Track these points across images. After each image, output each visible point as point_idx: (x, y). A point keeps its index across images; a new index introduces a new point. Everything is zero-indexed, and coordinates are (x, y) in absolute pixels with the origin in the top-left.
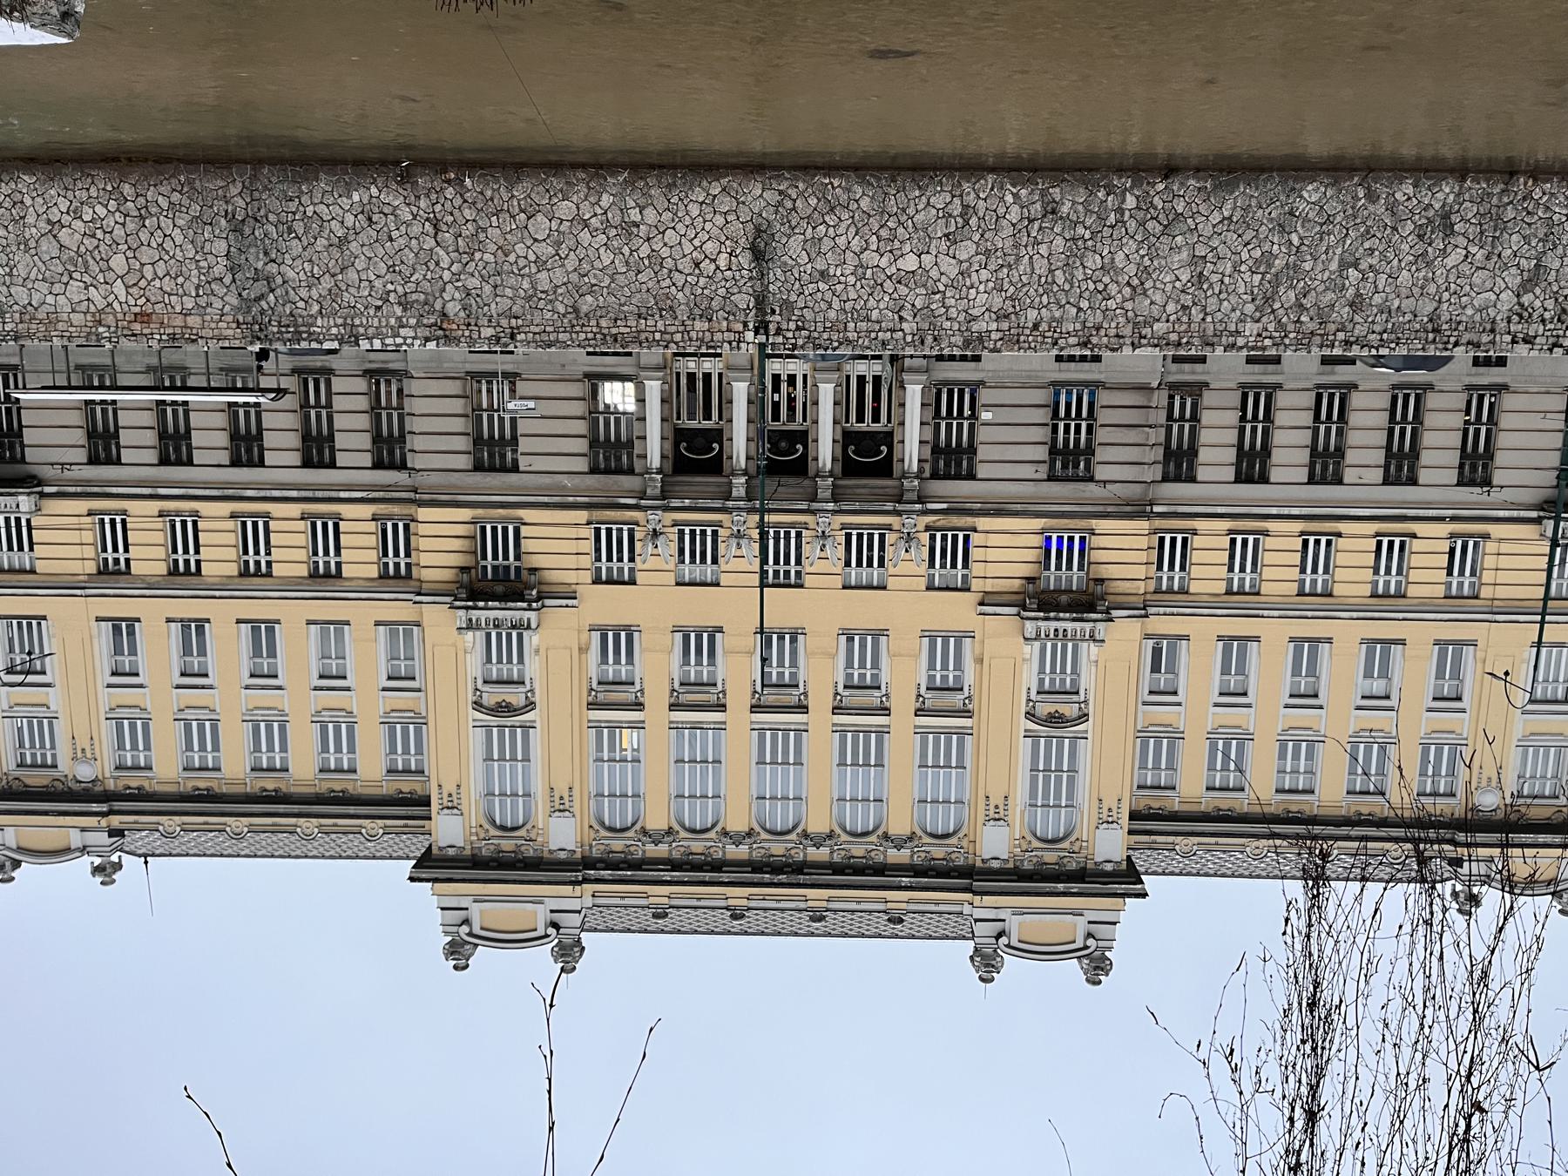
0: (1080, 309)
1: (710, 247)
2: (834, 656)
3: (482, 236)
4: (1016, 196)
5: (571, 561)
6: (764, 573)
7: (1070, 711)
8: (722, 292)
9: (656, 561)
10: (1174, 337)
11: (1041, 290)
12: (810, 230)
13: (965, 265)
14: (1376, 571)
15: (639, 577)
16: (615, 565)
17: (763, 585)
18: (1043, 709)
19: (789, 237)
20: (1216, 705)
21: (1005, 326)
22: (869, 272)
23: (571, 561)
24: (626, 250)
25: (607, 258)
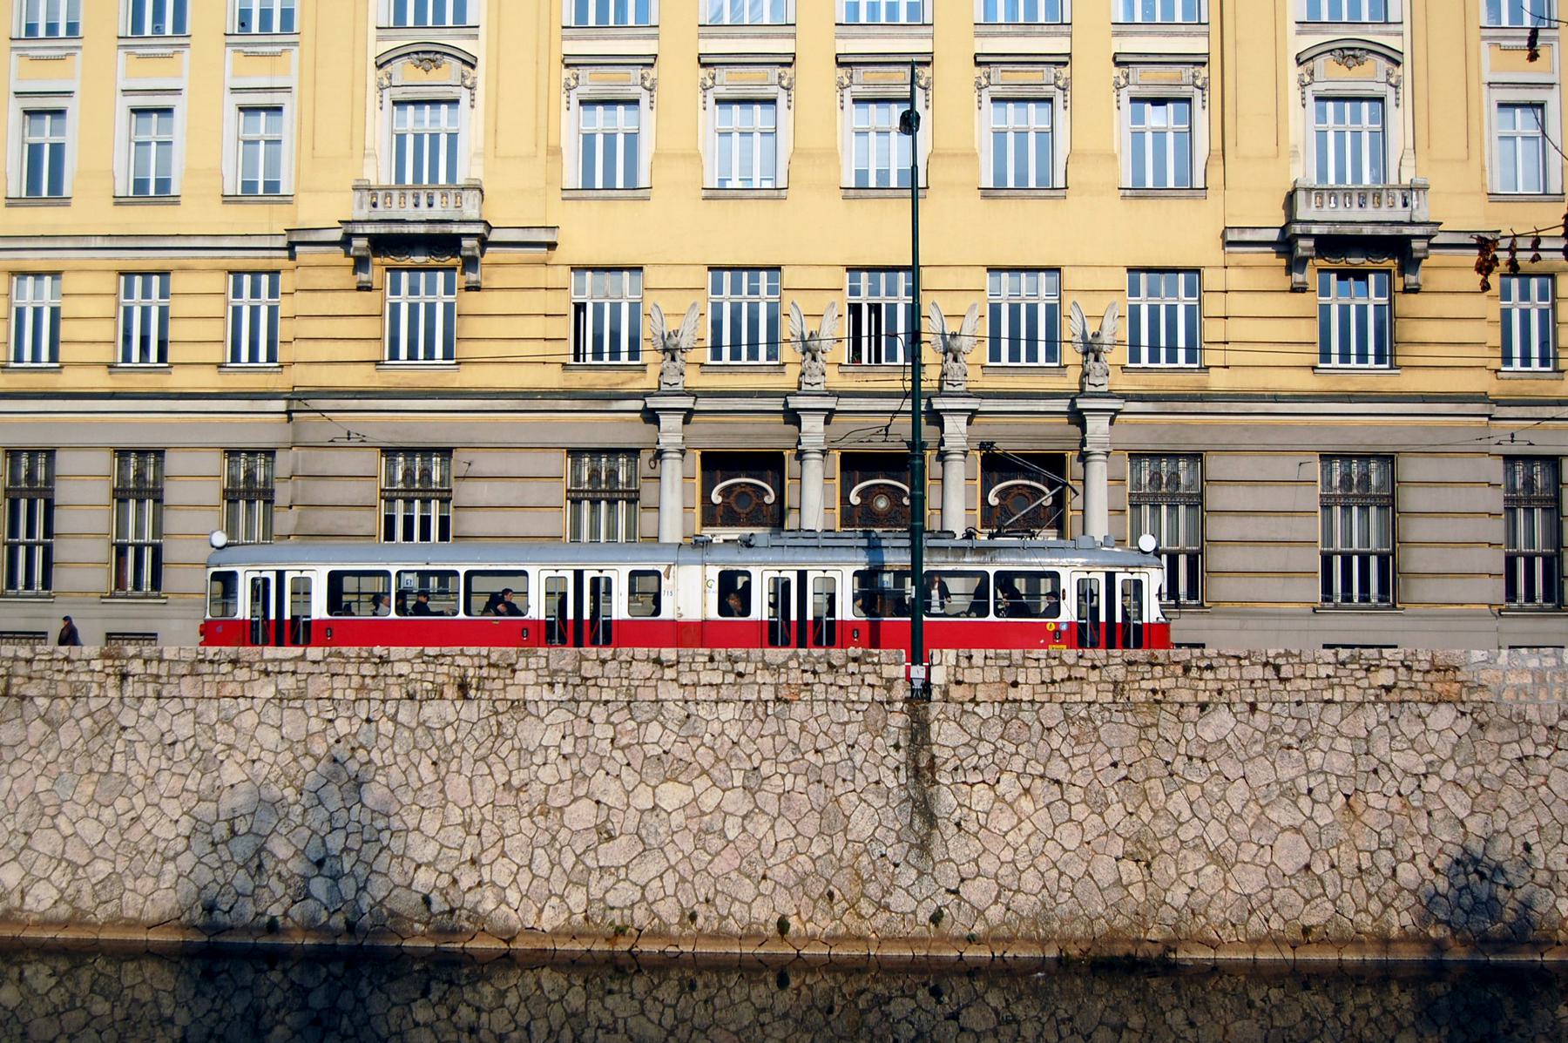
0: (393, 719)
1: (1004, 821)
2: (797, 152)
3: (1388, 836)
4: (503, 901)
5: (1237, 304)
6: (915, 290)
7: (404, 72)
8: (984, 749)
9: (1099, 306)
10: (243, 674)
11: (457, 749)
12: (838, 847)
13: (581, 791)
14: (164, 313)
15: (1124, 279)
16: (422, 300)
17: (914, 270)
18: (450, 70)
19: (873, 838)
20: (177, 91)
21: (513, 693)
22: (738, 781)
23: (1237, 304)
24: (1146, 815)
25: (1178, 803)
